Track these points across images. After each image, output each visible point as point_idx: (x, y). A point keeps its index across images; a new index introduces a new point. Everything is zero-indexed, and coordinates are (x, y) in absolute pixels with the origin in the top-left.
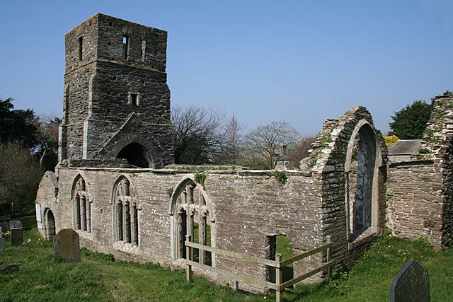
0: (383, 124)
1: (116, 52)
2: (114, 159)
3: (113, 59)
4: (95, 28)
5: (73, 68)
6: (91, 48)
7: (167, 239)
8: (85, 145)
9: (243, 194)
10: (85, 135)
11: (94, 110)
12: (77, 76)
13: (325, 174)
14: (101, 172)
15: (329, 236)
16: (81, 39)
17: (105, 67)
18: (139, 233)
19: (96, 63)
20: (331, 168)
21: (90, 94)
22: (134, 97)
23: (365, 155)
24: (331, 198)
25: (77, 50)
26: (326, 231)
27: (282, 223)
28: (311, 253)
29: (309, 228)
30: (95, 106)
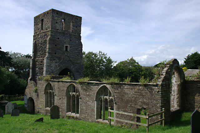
0: (181, 62)
1: (58, 26)
2: (58, 76)
3: (58, 30)
4: (50, 16)
5: (38, 33)
6: (48, 24)
7: (93, 110)
8: (45, 69)
9: (128, 92)
10: (45, 64)
11: (49, 53)
12: (40, 37)
13: (162, 85)
14: (61, 83)
15: (163, 109)
16: (42, 20)
17: (54, 31)
18: (79, 108)
19: (50, 32)
20: (164, 83)
21: (48, 46)
22: (67, 47)
23: (176, 78)
24: (164, 94)
25: (40, 25)
26: (162, 107)
27: (144, 103)
28: (156, 115)
29: (155, 105)
30: (49, 51)
